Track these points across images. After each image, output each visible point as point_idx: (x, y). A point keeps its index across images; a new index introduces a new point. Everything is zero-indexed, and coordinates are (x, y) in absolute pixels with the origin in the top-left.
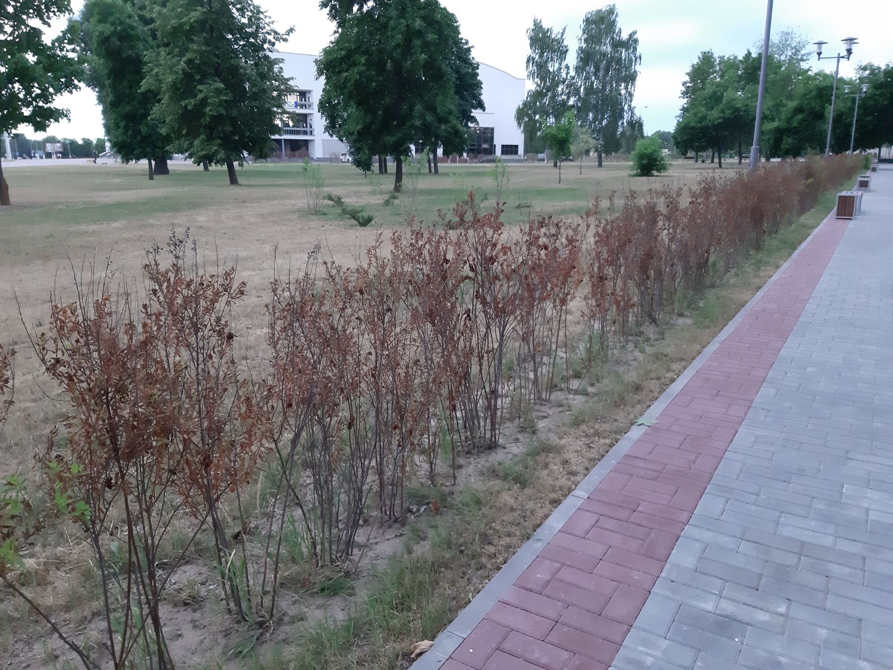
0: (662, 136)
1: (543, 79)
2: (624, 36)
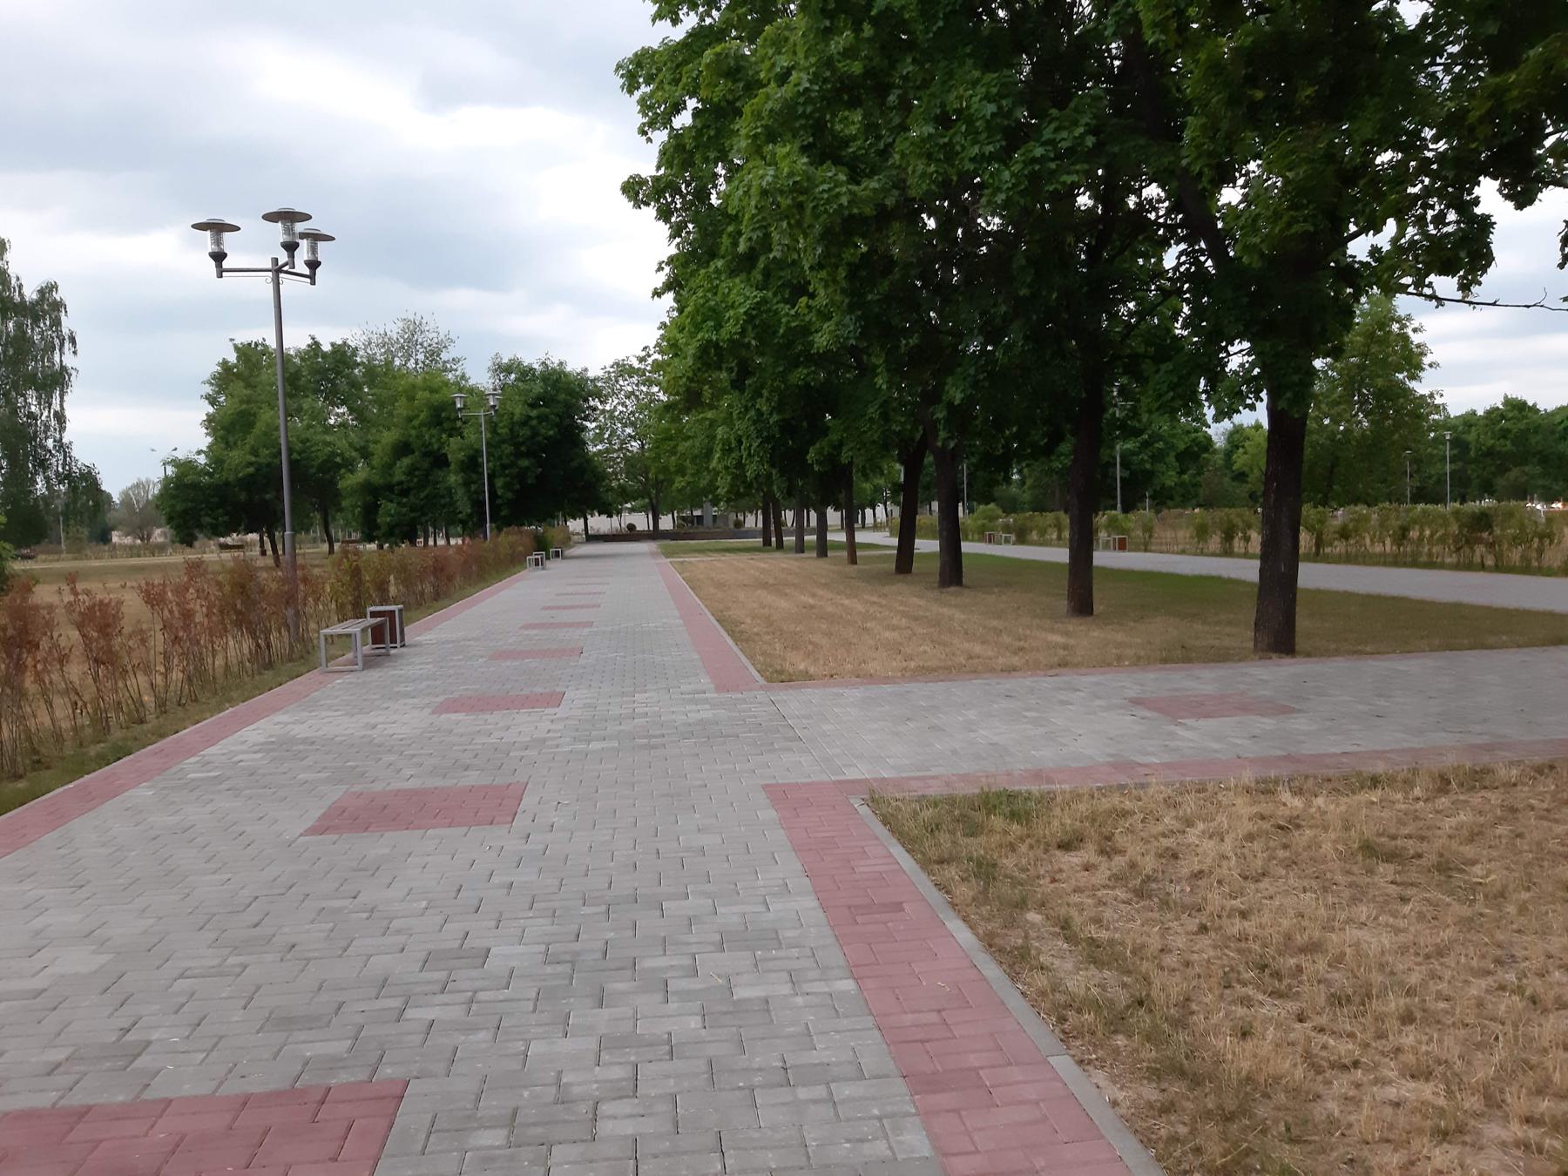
2: (30, 294)
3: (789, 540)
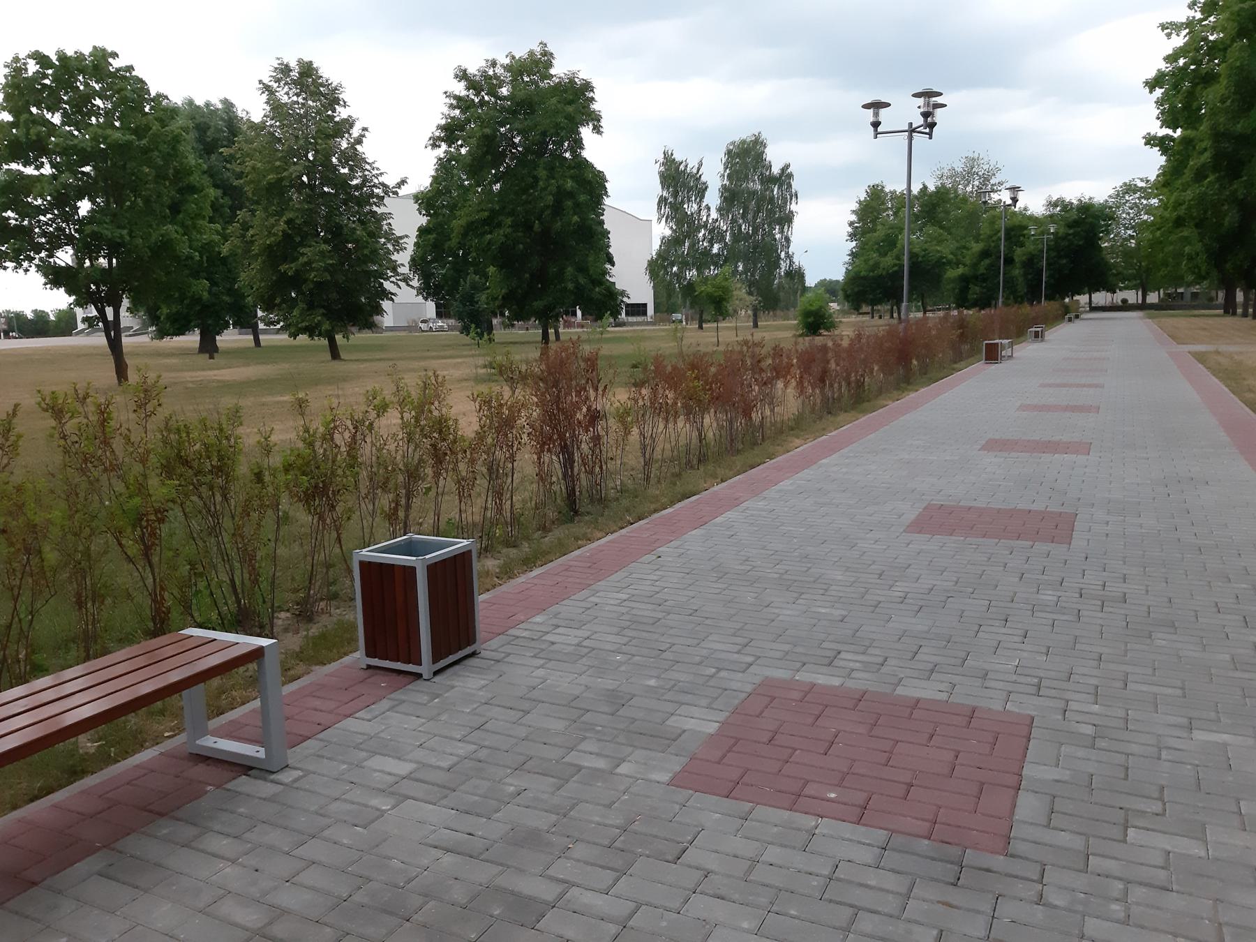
0: (829, 288)
1: (679, 223)
2: (776, 170)
3: (1239, 311)
